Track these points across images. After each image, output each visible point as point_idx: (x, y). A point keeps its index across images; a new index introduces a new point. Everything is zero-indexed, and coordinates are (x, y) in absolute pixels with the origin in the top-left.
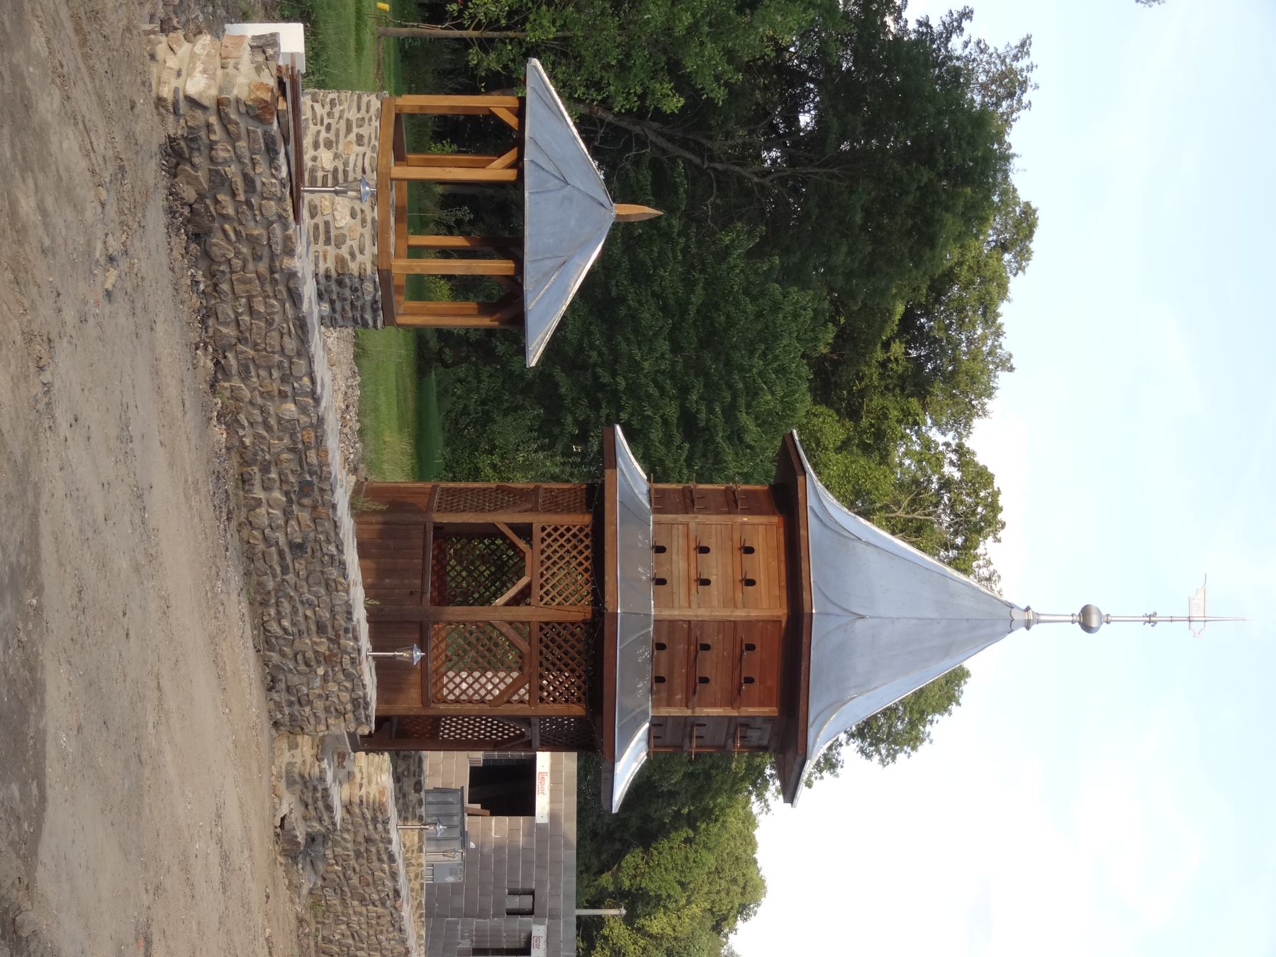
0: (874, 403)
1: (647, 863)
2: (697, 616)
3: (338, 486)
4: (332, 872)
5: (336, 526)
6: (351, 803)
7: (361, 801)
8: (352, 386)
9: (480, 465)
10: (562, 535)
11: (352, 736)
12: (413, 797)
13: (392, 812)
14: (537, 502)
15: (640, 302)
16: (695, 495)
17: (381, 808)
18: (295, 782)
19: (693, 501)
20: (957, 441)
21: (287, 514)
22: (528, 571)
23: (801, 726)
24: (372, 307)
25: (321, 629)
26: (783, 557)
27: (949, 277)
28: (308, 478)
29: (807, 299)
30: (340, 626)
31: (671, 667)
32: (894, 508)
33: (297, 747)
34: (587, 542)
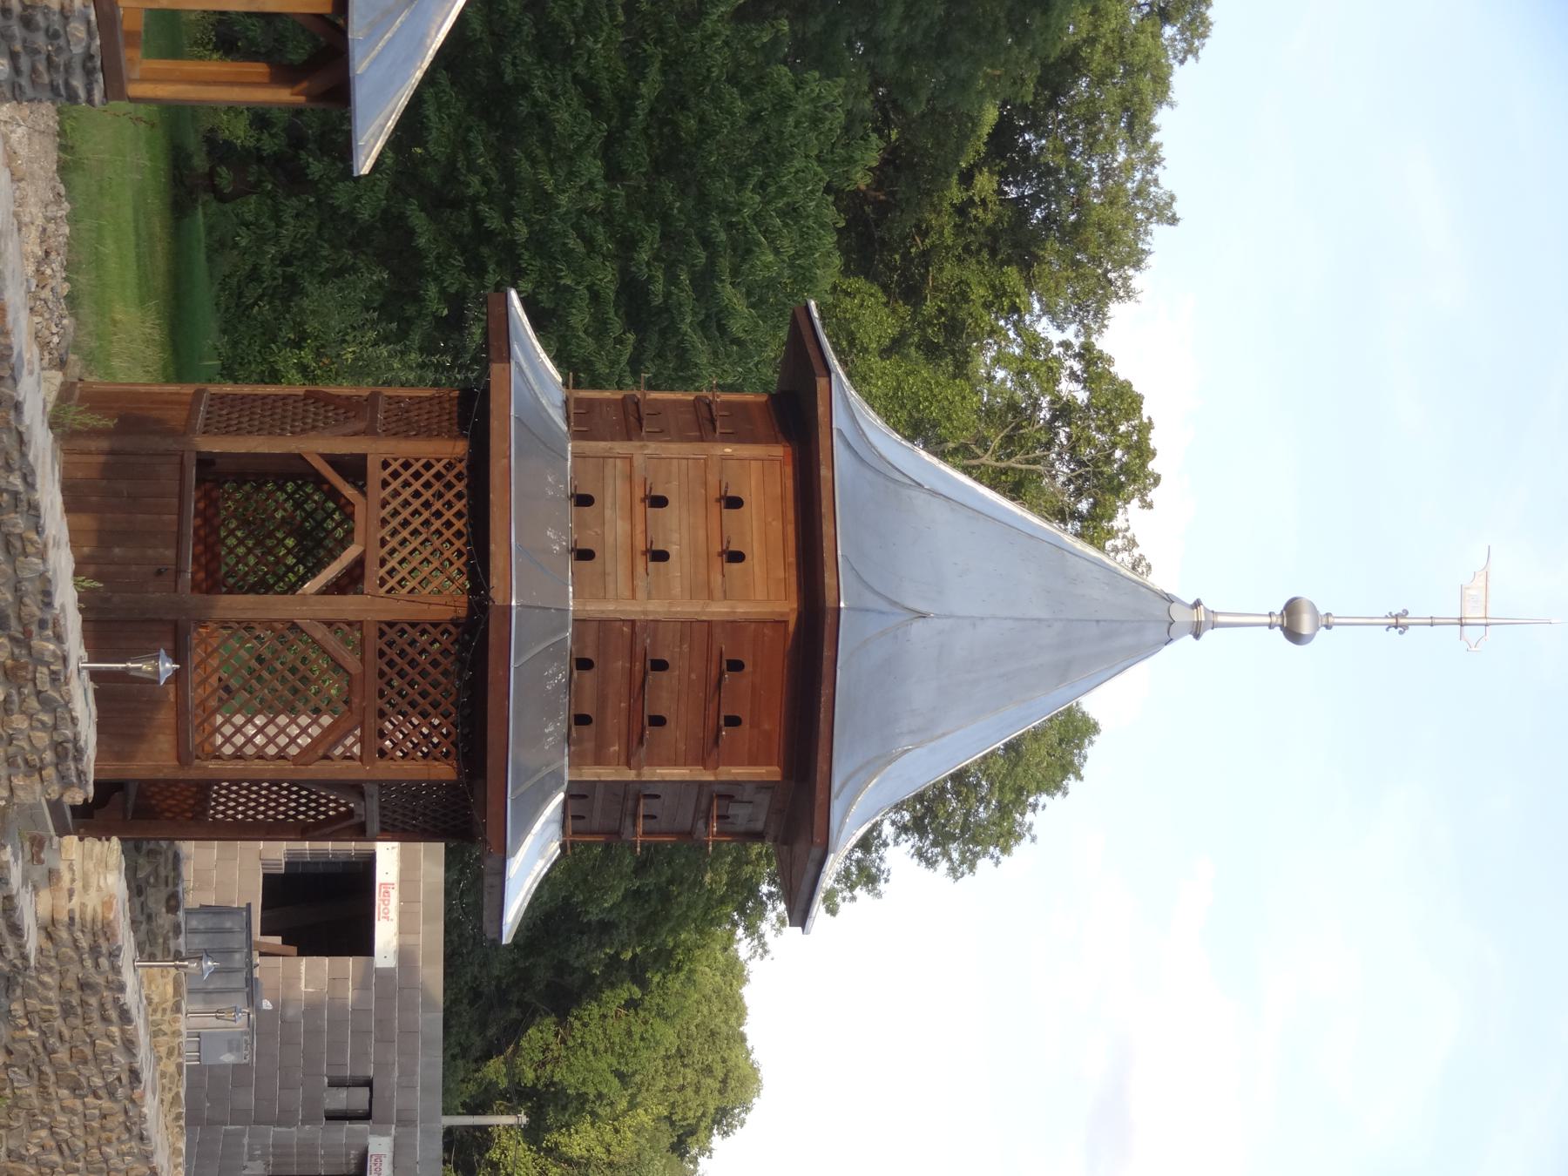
0: (946, 274)
1: (564, 1041)
2: (645, 613)
3: (25, 372)
4: (22, 1040)
6: (53, 921)
7: (72, 919)
8: (54, 218)
9: (280, 366)
10: (417, 475)
11: (55, 806)
12: (164, 920)
13: (126, 939)
14: (374, 419)
15: (553, 95)
16: (644, 410)
17: (104, 930)
19: (639, 420)
20: (1082, 339)
23: (820, 797)
24: (84, 66)
26: (791, 515)
27: (1072, 63)
29: (836, 92)
30: (32, 616)
31: (602, 700)
32: (979, 451)
34: (460, 487)
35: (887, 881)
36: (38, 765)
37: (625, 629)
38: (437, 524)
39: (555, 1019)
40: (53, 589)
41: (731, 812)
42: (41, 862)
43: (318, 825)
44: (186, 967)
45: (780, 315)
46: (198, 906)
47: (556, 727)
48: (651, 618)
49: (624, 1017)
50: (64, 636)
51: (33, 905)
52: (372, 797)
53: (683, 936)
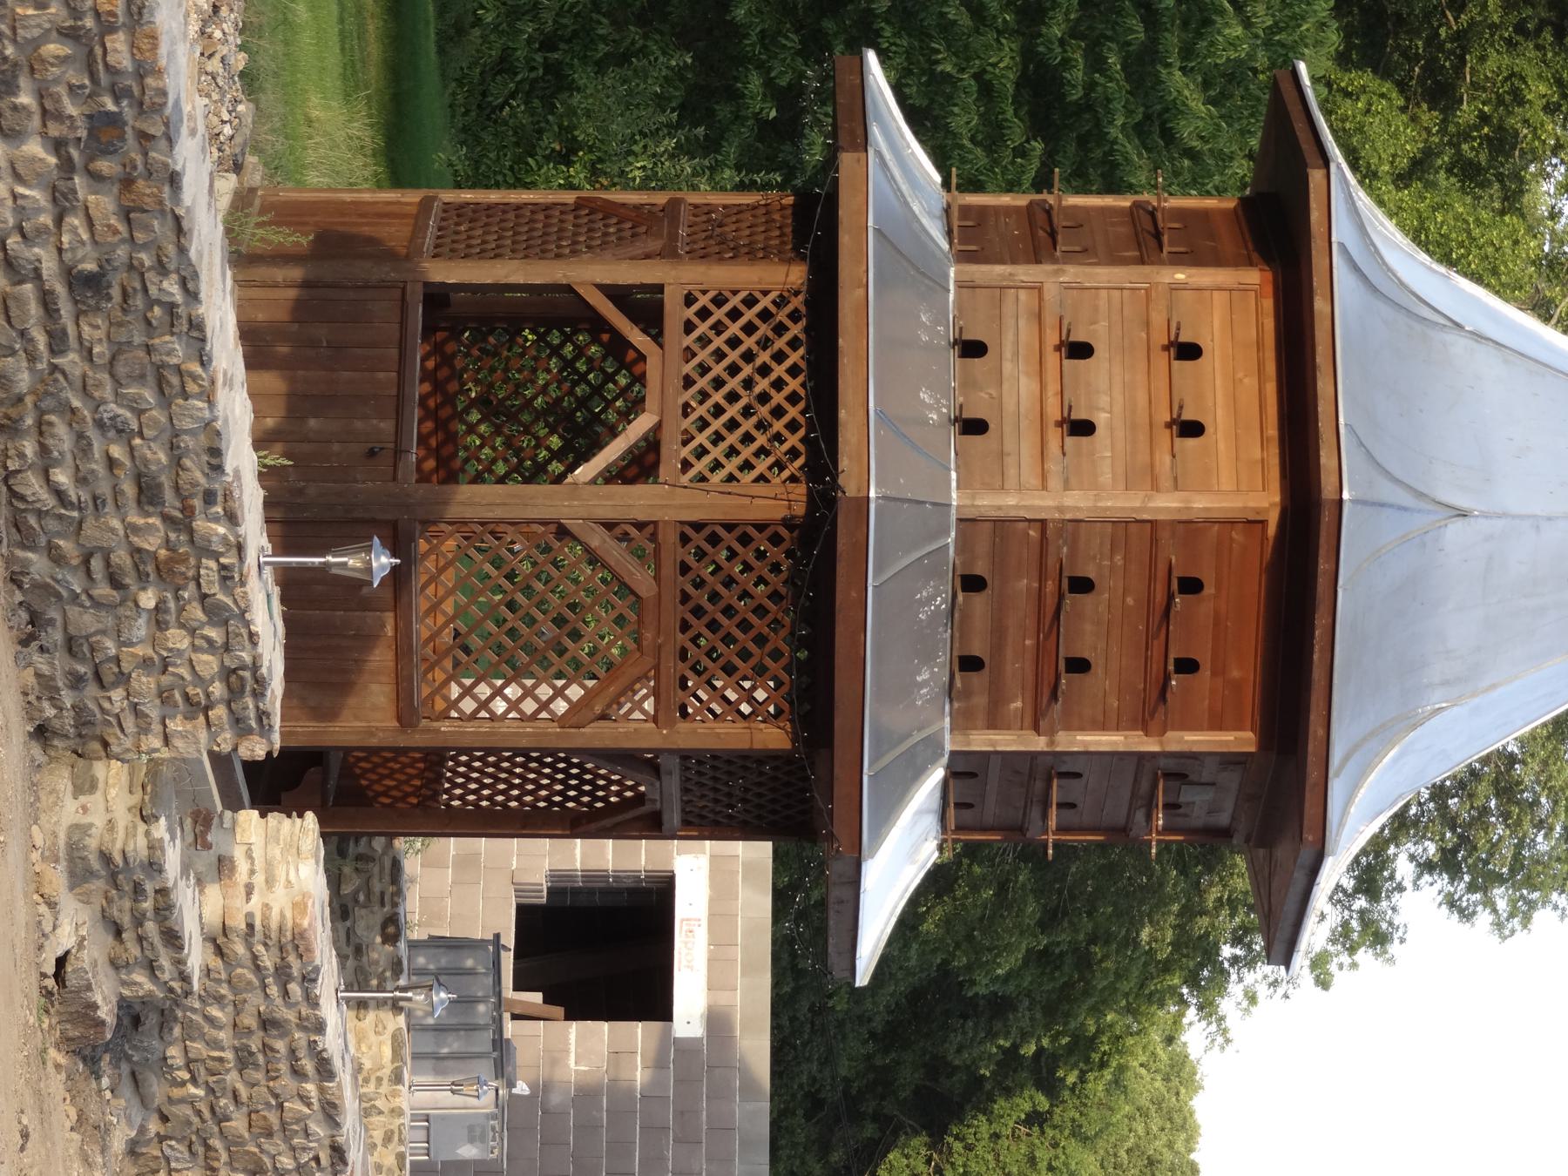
2: (1060, 509)
3: (184, 130)
4: (182, 1101)
5: (180, 229)
6: (225, 930)
7: (250, 926)
10: (734, 315)
11: (221, 762)
12: (379, 952)
14: (673, 237)
17: (297, 943)
18: (90, 874)
19: (1053, 235)
21: (62, 202)
22: (652, 402)
23: (1313, 775)
25: (148, 493)
26: (1271, 368)
28: (111, 106)
30: (195, 484)
31: (998, 633)
33: (92, 787)
34: (796, 330)
35: (1402, 941)
36: (203, 702)
37: (1032, 533)
38: (763, 384)
39: (926, 1139)
40: (223, 446)
41: (1182, 799)
42: (208, 846)
43: (595, 815)
44: (409, 999)
45: (1252, 115)
46: (426, 937)
47: (932, 673)
48: (1068, 516)
49: (1024, 1138)
50: (239, 514)
51: (197, 905)
52: (670, 773)
53: (1109, 1018)
